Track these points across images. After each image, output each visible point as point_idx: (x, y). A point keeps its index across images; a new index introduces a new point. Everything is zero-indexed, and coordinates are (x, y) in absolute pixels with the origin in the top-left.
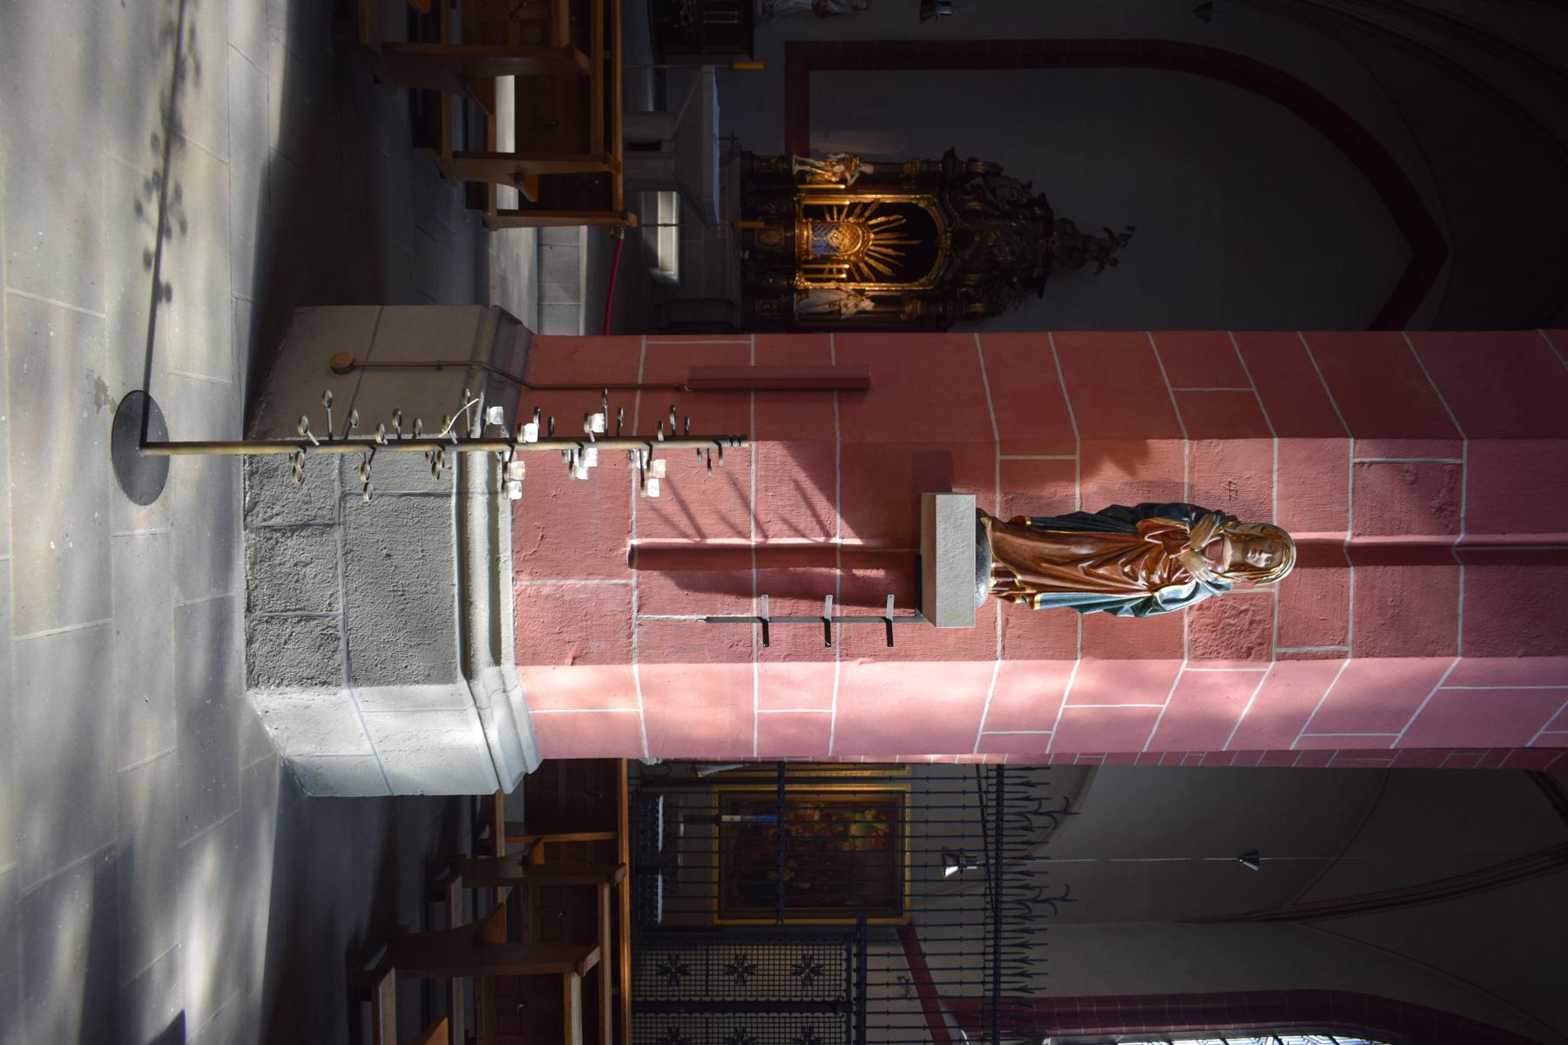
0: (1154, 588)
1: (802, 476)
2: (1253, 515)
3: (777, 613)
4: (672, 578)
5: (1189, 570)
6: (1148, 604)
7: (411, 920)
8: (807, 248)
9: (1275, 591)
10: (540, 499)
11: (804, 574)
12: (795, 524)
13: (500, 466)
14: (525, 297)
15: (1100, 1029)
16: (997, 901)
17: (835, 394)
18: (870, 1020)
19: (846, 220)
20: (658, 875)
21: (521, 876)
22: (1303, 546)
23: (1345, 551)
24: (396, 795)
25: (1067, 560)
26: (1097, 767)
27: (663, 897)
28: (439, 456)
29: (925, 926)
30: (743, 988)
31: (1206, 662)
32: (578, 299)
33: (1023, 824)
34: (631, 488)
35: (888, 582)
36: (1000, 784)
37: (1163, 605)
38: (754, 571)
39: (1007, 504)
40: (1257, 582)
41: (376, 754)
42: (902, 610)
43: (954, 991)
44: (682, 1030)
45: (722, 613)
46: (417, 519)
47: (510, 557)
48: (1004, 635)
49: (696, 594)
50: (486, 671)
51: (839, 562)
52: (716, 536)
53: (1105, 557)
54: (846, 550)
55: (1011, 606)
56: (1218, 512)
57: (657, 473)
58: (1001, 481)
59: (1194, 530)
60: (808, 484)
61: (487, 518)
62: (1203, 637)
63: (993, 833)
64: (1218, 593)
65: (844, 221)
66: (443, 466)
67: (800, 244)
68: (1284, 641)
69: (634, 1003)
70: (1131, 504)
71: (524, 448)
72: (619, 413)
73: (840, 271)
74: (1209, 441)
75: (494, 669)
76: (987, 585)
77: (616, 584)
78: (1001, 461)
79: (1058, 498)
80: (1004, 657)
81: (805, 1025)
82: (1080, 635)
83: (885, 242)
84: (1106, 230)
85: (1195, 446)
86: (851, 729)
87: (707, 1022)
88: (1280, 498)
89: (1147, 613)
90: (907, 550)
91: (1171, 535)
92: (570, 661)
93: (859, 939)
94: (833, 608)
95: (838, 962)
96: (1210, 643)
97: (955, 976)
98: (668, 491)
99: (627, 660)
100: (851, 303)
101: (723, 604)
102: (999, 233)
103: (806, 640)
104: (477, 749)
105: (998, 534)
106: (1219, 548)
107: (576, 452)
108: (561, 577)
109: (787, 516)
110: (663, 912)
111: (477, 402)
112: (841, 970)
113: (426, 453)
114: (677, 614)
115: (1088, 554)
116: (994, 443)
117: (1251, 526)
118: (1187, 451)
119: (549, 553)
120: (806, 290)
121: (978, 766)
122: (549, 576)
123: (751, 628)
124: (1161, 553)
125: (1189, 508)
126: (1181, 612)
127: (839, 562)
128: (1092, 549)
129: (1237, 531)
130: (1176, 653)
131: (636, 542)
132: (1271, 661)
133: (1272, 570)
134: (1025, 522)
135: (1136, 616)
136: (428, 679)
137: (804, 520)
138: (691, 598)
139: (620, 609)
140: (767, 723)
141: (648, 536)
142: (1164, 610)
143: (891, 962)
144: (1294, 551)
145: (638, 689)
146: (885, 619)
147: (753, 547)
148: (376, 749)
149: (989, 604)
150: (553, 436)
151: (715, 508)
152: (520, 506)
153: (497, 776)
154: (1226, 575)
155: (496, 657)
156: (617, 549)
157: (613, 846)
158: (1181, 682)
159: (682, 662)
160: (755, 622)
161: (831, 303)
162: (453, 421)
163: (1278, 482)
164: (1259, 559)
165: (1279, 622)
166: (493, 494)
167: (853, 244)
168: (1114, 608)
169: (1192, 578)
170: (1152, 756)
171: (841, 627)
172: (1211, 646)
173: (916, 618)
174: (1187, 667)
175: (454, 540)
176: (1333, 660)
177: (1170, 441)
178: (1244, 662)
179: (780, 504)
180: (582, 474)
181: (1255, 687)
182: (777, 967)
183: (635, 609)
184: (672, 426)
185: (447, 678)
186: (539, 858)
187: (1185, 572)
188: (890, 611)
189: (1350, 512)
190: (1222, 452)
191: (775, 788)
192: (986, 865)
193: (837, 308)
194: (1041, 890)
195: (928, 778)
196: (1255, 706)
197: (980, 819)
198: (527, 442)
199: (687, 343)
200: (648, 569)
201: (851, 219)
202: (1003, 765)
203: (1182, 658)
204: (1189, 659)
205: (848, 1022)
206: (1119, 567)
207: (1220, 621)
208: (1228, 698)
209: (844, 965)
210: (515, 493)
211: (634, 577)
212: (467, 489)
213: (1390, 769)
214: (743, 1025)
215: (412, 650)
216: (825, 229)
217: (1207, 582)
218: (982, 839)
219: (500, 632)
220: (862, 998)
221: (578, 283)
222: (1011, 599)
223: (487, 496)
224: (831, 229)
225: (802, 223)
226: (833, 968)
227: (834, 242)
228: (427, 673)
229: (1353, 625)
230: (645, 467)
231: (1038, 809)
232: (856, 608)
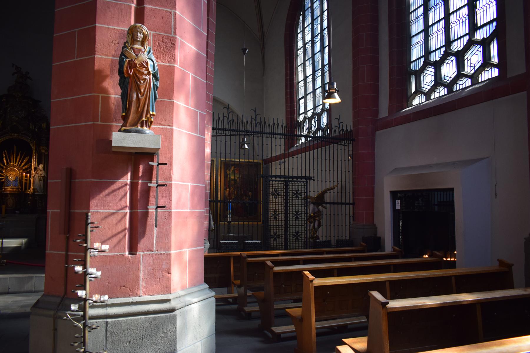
0: (149, 73)
1: (104, 193)
2: (124, 36)
3: (154, 203)
4: (140, 240)
5: (143, 61)
6: (155, 76)
7: (257, 323)
8: (16, 189)
9: (152, 32)
10: (109, 288)
11: (140, 193)
12: (122, 196)
13: (95, 304)
14: (31, 298)
15: (295, 103)
16: (256, 133)
17: (73, 180)
18: (291, 174)
19: (4, 173)
20: (245, 242)
21: (244, 288)
22: (136, 21)
23: (139, 7)
24: (215, 332)
25: (138, 102)
26: (214, 97)
27: (253, 240)
28: (90, 327)
29: (263, 156)
30: (281, 214)
31: (176, 58)
32: (32, 277)
33: (231, 122)
34: (106, 255)
35: (144, 164)
36: (219, 129)
37: (155, 71)
38: (139, 211)
39: (117, 121)
40: (148, 38)
41: (201, 340)
42: (154, 160)
43: (283, 148)
44: (293, 234)
45: (154, 222)
46: (116, 333)
47: (131, 298)
48: (165, 125)
49: (147, 231)
50: (173, 304)
51: (137, 181)
52: (126, 224)
53: (137, 89)
54: (132, 178)
55: (154, 122)
56: (123, 48)
57: (99, 246)
58: (108, 122)
59: (129, 57)
60: (107, 191)
61: (116, 307)
62: (168, 58)
63: (234, 132)
64: (152, 52)
65: (5, 174)
66: (94, 325)
67: (14, 191)
68: (170, 32)
69: (285, 249)
70: (118, 78)
71: (88, 296)
72: (75, 260)
73: (26, 176)
74: (96, 48)
75: (172, 302)
76: (146, 130)
77: (142, 260)
78: (101, 122)
79: (115, 103)
80: (172, 126)
81: (292, 195)
82: (165, 100)
83: (14, 160)
84: (13, 74)
85: (98, 53)
86: (198, 177)
87: (291, 226)
88: (118, 26)
89: (158, 77)
90: (133, 157)
91: (130, 65)
92: (170, 275)
93: (268, 177)
94: (153, 183)
95: (273, 184)
96: (170, 57)
97: (278, 147)
98: (108, 242)
99: (170, 255)
100: (40, 172)
101: (150, 222)
102: (13, 115)
103: (164, 193)
104: (200, 305)
105: (128, 125)
106: (136, 50)
107: (90, 276)
108: (139, 279)
109: (119, 199)
110: (257, 240)
111: (69, 314)
112: (279, 183)
113: (89, 332)
114: (154, 238)
115: (136, 94)
116: (94, 124)
117: (128, 38)
118: (100, 56)
119: (130, 284)
120: (34, 189)
121: (212, 136)
122: (139, 284)
123: (159, 212)
124: (137, 70)
125: (120, 58)
126: (158, 65)
127: (137, 181)
128: (134, 93)
129: (130, 43)
130: (173, 68)
131: (127, 253)
132: (176, 37)
133: (144, 33)
134: (124, 115)
135: (159, 80)
136: (175, 324)
137: (121, 193)
138: (148, 233)
139: (152, 258)
140: (193, 207)
141: (125, 248)
142: (157, 71)
143: (274, 167)
144: (138, 24)
145: (180, 251)
146: (157, 166)
147: (130, 211)
148: (199, 340)
149: (153, 130)
150: (83, 285)
151: (115, 225)
152: (112, 295)
153: (209, 298)
154: (145, 48)
155: (167, 301)
156: (130, 259)
157: (235, 257)
158: (183, 68)
159: (171, 236)
160: (157, 210)
161: (40, 180)
162: (75, 322)
163: (112, 26)
164: (140, 37)
165: (163, 33)
166: (107, 306)
167: (15, 171)
168: (156, 87)
169: (146, 60)
170: (207, 78)
171: (160, 181)
172: (170, 56)
173: (157, 155)
174: (177, 65)
175: (124, 319)
176: (177, 17)
177: (95, 62)
178: (176, 46)
179: (114, 201)
180: (99, 273)
181: (185, 44)
182: (275, 203)
183: (151, 253)
184: (81, 241)
185: (175, 317)
186: (238, 282)
187: (144, 62)
188: (155, 164)
189: (125, 3)
190: (100, 44)
191: (219, 204)
192: (244, 135)
193: (42, 178)
194: (253, 118)
195: (216, 153)
196: (191, 44)
197: (220, 137)
198: (86, 294)
199: (49, 237)
200: (137, 248)
201: (4, 171)
202: (212, 128)
203: (174, 66)
204: (175, 64)
205: (291, 181)
206: (141, 84)
207: (162, 52)
208: (188, 53)
209: (274, 182)
210: (106, 297)
211: (140, 253)
212: (105, 315)
213: (217, 3)
214: (292, 214)
215: (164, 331)
216: (8, 181)
217: (148, 55)
218: (236, 136)
219: (159, 300)
220: (284, 177)
221: (25, 277)
222: (151, 122)
223: (108, 308)
224: (8, 179)
225: (4, 190)
226: (275, 186)
227: (14, 178)
228: (172, 325)
229: (165, 8)
230: (97, 250)
231: (227, 117)
232: (153, 175)
